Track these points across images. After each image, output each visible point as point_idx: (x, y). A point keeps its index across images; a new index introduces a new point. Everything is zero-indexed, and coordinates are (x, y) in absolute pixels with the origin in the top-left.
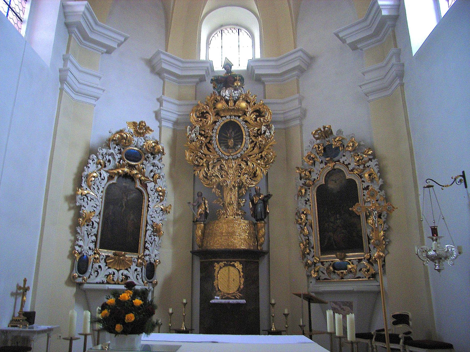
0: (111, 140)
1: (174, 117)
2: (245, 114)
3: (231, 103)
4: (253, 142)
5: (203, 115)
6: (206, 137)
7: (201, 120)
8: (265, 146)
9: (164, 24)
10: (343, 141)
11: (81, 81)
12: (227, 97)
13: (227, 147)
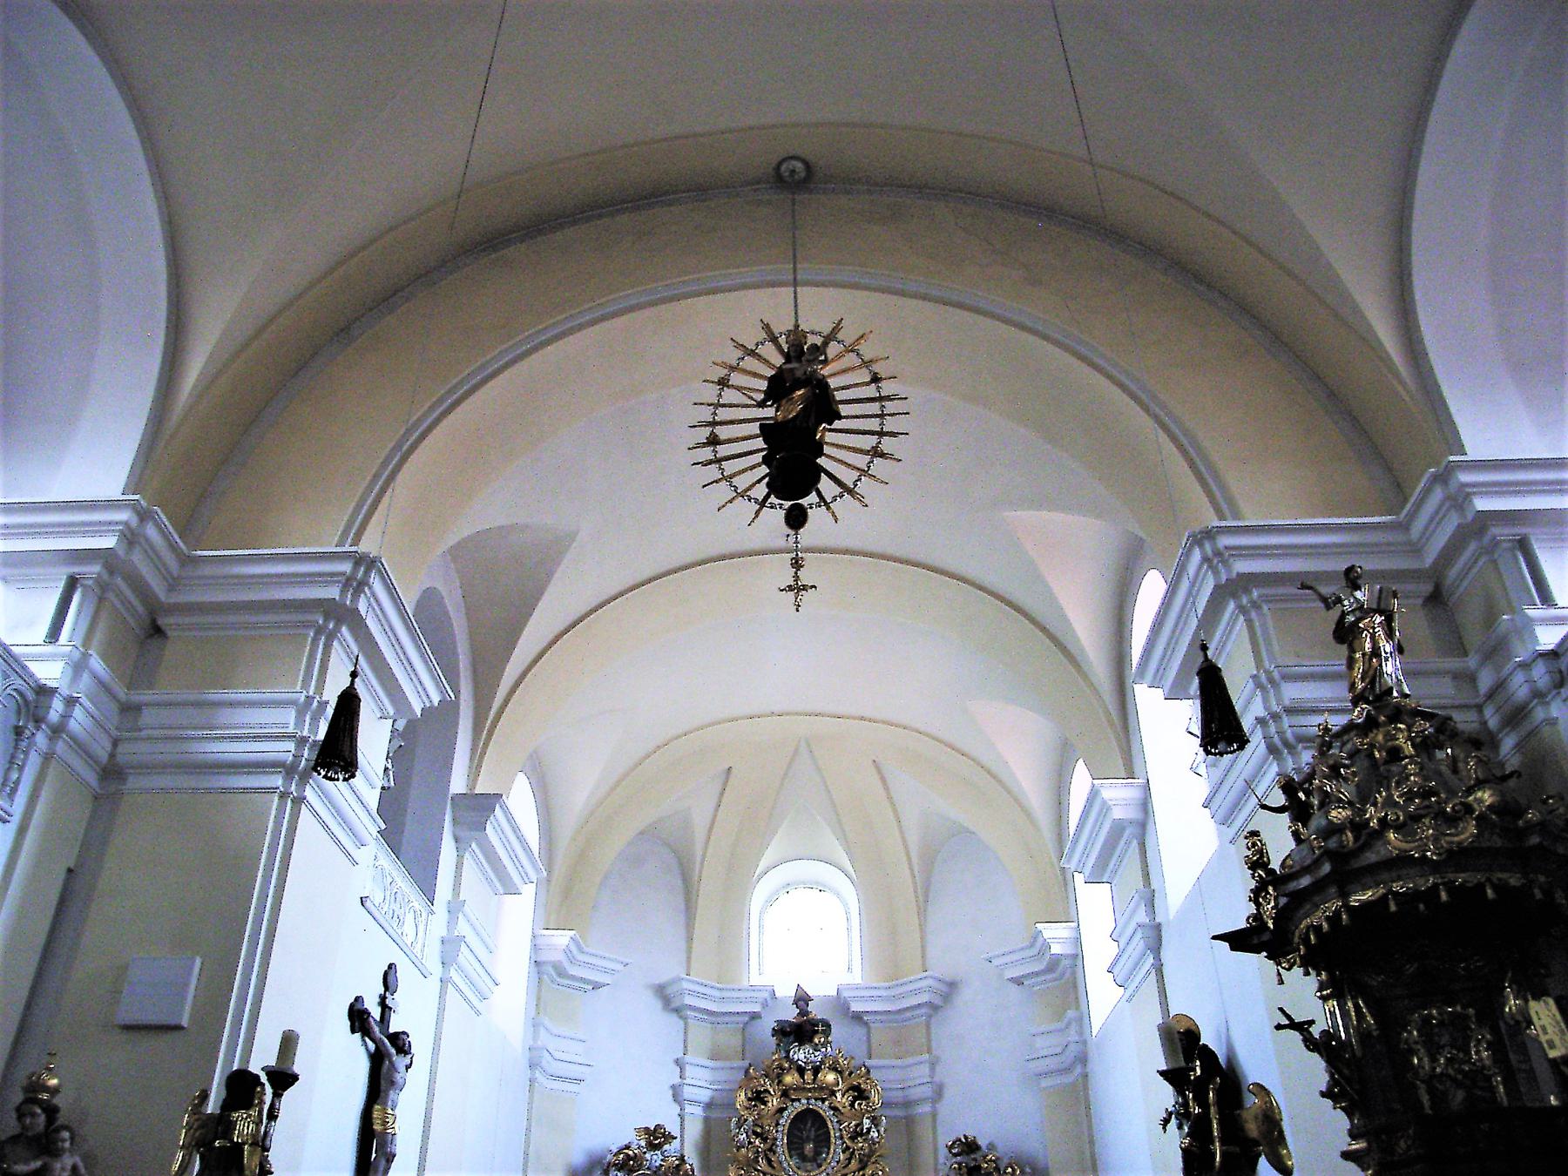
0: (612, 1164)
1: (705, 1096)
2: (833, 1093)
3: (809, 1076)
4: (848, 1148)
5: (759, 1097)
6: (764, 1140)
7: (755, 1106)
8: (870, 1156)
9: (682, 907)
10: (998, 1162)
11: (557, 1055)
12: (800, 1063)
13: (803, 1158)
